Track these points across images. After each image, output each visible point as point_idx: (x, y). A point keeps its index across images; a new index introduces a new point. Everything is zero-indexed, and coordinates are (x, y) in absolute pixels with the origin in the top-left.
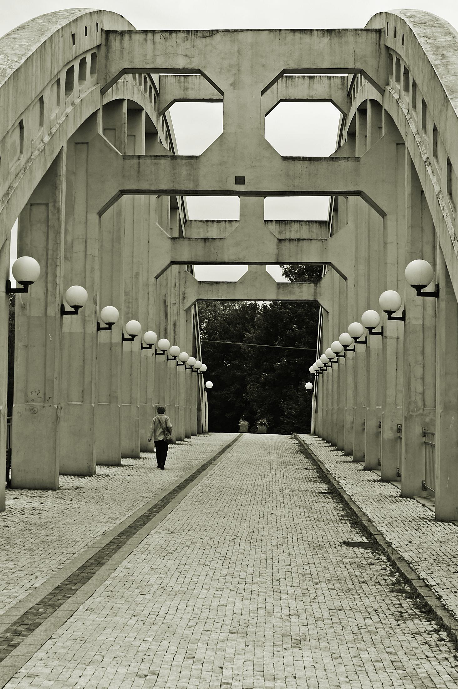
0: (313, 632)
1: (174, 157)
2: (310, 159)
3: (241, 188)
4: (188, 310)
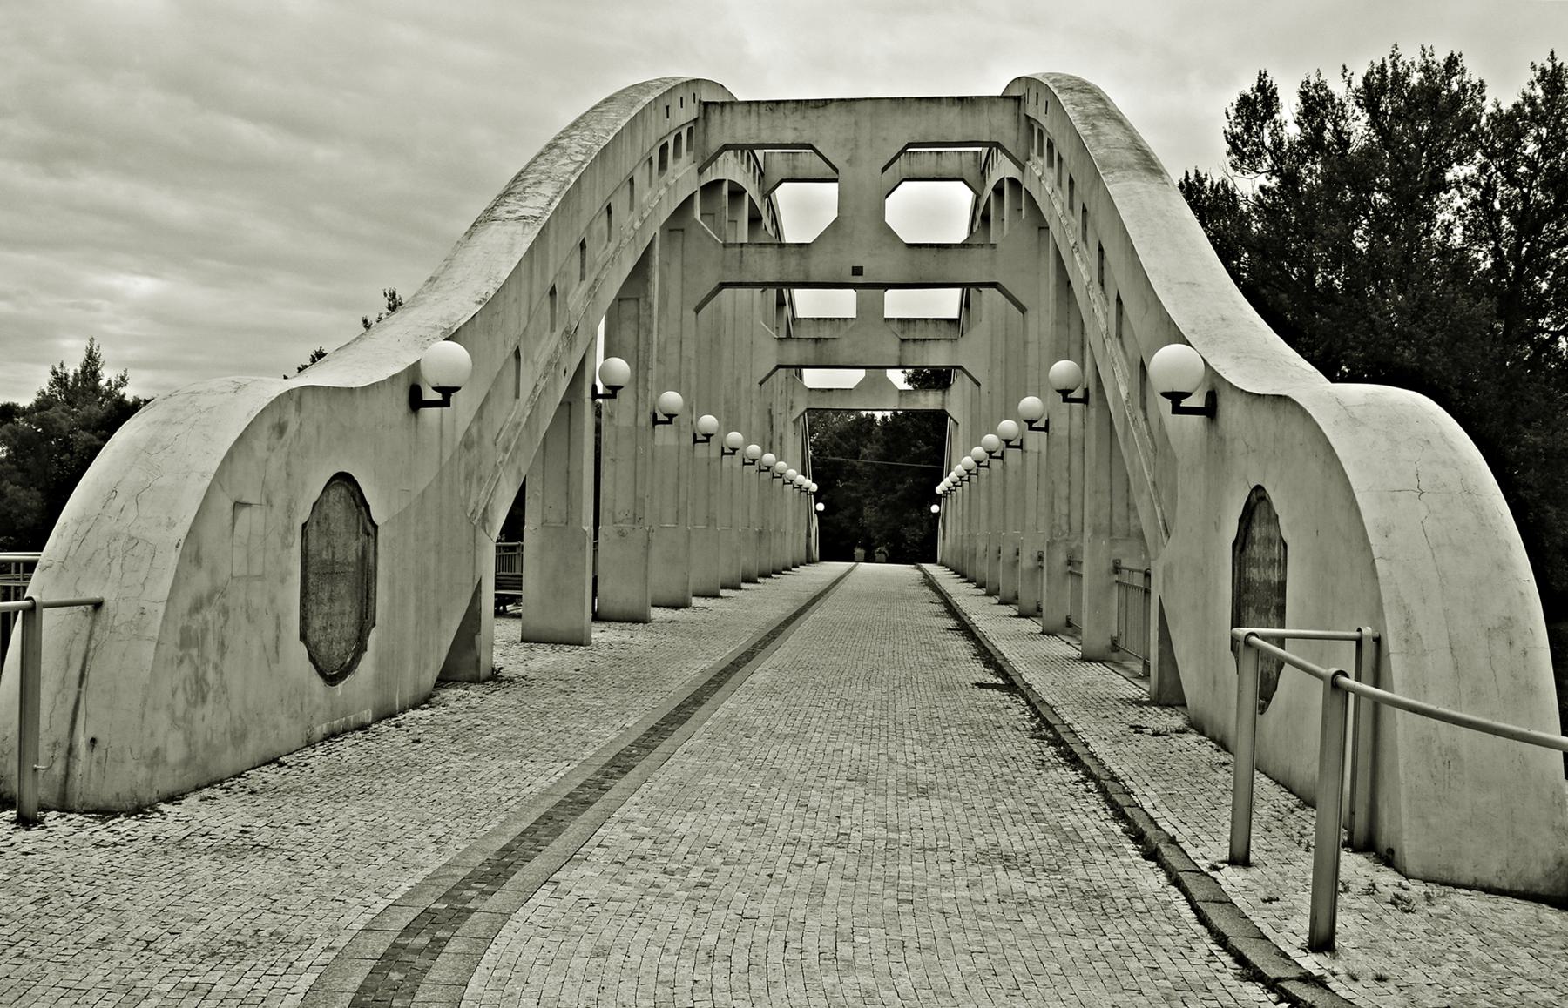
0: (942, 780)
1: (782, 245)
2: (939, 246)
3: (859, 280)
4: (796, 422)
